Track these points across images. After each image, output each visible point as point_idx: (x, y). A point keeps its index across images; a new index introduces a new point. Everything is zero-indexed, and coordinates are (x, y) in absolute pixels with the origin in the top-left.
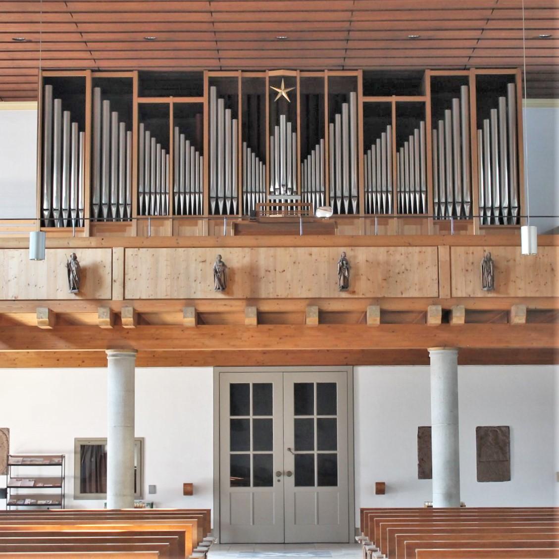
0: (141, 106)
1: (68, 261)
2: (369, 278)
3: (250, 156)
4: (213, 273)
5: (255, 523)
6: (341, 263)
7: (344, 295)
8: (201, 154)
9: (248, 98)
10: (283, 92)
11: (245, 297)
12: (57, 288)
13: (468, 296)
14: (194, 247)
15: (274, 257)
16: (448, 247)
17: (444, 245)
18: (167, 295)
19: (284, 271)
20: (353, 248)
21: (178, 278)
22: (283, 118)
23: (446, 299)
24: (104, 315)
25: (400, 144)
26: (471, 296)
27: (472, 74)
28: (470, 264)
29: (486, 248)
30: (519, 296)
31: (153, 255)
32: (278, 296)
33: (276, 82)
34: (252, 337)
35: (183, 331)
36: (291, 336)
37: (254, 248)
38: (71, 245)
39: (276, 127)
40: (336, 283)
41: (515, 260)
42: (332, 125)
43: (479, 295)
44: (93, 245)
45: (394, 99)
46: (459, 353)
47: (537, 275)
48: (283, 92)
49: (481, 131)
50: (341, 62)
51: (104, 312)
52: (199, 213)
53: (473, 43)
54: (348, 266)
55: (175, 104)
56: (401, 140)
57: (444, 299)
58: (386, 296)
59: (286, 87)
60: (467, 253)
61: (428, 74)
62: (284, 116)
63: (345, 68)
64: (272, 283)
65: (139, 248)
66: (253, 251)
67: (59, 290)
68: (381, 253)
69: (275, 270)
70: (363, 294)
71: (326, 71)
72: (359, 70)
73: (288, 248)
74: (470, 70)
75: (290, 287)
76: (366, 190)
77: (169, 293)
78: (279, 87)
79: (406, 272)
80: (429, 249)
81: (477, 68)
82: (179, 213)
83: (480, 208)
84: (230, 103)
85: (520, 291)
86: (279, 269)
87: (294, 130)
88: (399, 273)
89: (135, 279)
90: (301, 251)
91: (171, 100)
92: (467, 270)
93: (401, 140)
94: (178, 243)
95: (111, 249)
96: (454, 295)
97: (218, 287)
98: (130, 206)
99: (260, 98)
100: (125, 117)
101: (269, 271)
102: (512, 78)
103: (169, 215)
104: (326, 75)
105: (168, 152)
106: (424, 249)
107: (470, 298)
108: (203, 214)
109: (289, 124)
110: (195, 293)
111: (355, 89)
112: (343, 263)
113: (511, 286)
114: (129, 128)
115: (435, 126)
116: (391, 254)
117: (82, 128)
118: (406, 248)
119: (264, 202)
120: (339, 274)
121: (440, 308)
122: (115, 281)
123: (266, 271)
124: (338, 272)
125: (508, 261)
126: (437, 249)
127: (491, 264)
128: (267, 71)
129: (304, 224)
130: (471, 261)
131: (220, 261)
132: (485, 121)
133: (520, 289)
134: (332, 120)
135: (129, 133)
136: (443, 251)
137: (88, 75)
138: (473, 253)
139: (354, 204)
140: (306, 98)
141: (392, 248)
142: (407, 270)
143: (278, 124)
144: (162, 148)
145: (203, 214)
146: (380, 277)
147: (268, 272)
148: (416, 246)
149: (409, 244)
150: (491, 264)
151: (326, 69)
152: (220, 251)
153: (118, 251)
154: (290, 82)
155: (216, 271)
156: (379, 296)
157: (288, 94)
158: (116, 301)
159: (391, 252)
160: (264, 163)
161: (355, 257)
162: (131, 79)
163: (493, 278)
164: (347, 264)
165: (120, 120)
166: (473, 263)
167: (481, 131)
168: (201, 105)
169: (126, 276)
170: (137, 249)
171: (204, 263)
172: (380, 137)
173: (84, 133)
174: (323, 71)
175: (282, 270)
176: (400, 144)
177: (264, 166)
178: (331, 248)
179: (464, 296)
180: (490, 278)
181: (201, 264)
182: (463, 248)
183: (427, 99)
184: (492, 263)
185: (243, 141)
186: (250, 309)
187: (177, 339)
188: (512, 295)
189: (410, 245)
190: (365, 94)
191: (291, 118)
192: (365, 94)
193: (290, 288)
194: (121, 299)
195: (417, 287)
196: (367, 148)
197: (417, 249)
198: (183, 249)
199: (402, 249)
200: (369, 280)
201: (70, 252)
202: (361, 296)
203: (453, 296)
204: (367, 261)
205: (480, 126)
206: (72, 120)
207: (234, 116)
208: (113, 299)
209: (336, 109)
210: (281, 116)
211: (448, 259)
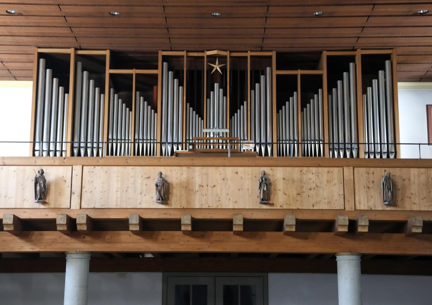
0: (111, 75)
1: (36, 175)
2: (286, 193)
3: (193, 114)
4: (155, 187)
5: (398, 56)
6: (261, 180)
7: (264, 207)
8: (156, 111)
9: (190, 73)
10: (217, 67)
11: (182, 207)
12: (24, 199)
13: (370, 209)
14: (140, 166)
15: (207, 174)
16: (352, 168)
17: (349, 166)
18: (117, 205)
19: (215, 186)
20: (272, 168)
21: (127, 191)
22: (216, 85)
23: (351, 212)
24: (61, 220)
25: (304, 106)
26: (373, 209)
27: (358, 54)
28: (371, 182)
29: (386, 169)
30: (415, 209)
31: (107, 172)
32: (209, 206)
33: (212, 59)
34: (188, 241)
35: (130, 236)
36: (219, 241)
37: (190, 167)
38: (38, 163)
39: (212, 92)
40: (258, 197)
41: (409, 180)
42: (253, 91)
43: (380, 208)
44: (57, 163)
45: (299, 72)
46: (361, 258)
47: (429, 192)
48: (217, 67)
49: (365, 95)
50: (259, 42)
51: (61, 218)
52: (153, 155)
53: (361, 21)
54: (267, 182)
55: (137, 74)
56: (305, 102)
57: (349, 211)
58: (300, 208)
59: (219, 64)
60: (368, 173)
61: (325, 54)
62: (218, 84)
63: (263, 49)
64: (205, 196)
65: (95, 166)
66: (189, 169)
67: (26, 200)
68: (295, 172)
69: (208, 186)
70: (280, 206)
71: (249, 52)
72: (273, 51)
73: (218, 167)
74: (357, 51)
75: (220, 199)
76: (278, 139)
77: (119, 204)
78: (215, 64)
79: (316, 188)
80: (336, 169)
81: (362, 49)
82: (138, 154)
83: (365, 153)
84: (178, 75)
85: (415, 205)
86: (210, 184)
87: (225, 94)
88: (310, 189)
89: (91, 192)
90: (229, 170)
91: (133, 72)
92: (368, 188)
93: (305, 102)
94: (127, 162)
95: (71, 167)
96: (358, 208)
97: (158, 198)
98: (102, 148)
99: (200, 73)
100: (100, 84)
101: (203, 186)
102: (388, 57)
103: (131, 155)
104: (249, 54)
105: (131, 110)
106: (331, 169)
107: (371, 210)
108: (156, 155)
109: (221, 90)
110: (140, 203)
111: (270, 66)
112: (262, 180)
113: (407, 200)
114: (102, 91)
115: (330, 92)
116: (304, 173)
117: (66, 91)
118: (316, 168)
119: (202, 148)
120: (259, 188)
121: (347, 218)
122: (74, 193)
123: (200, 186)
124: (258, 187)
125: (404, 180)
126: (342, 169)
127: (391, 182)
128: (205, 51)
129: (232, 154)
130: (372, 180)
131: (161, 177)
132: (368, 88)
133: (415, 204)
134: (253, 88)
135: (102, 95)
136: (348, 171)
137: (71, 51)
138: (373, 173)
139: (269, 149)
140: (234, 72)
141: (305, 169)
142: (317, 186)
143: (213, 90)
144: (126, 107)
145: (156, 155)
146: (295, 193)
147: (201, 187)
148: (325, 167)
149: (319, 165)
150: (391, 182)
151: (249, 50)
152: (162, 169)
153: (77, 169)
154: (222, 59)
155: (157, 186)
156: (294, 208)
157: (221, 68)
158: (74, 210)
159: (304, 172)
160: (202, 119)
161: (273, 175)
162: (105, 56)
163: (392, 193)
164: (266, 180)
165: (95, 86)
166: (373, 182)
167: (365, 95)
168: (156, 76)
169: (83, 189)
170: (93, 167)
171: (148, 179)
172: (289, 101)
173: (68, 94)
174: (247, 52)
175: (213, 185)
176: (304, 106)
177: (202, 120)
178: (254, 168)
179: (366, 208)
180: (390, 194)
181: (146, 180)
182: (364, 169)
183: (324, 72)
184: (392, 181)
185: (187, 102)
186: (185, 217)
187: (125, 242)
188: (408, 209)
189: (320, 166)
190: (278, 68)
191: (223, 86)
192: (278, 68)
193: (219, 200)
194: (78, 208)
195: (326, 201)
196: (279, 108)
197: (326, 169)
198: (131, 167)
199: (314, 169)
200: (285, 194)
201: (38, 168)
202: (279, 208)
203: (356, 209)
204: (284, 179)
205: (365, 92)
206: (60, 85)
207: (181, 84)
208: (71, 208)
209: (256, 80)
210: (216, 84)
211: (352, 178)
